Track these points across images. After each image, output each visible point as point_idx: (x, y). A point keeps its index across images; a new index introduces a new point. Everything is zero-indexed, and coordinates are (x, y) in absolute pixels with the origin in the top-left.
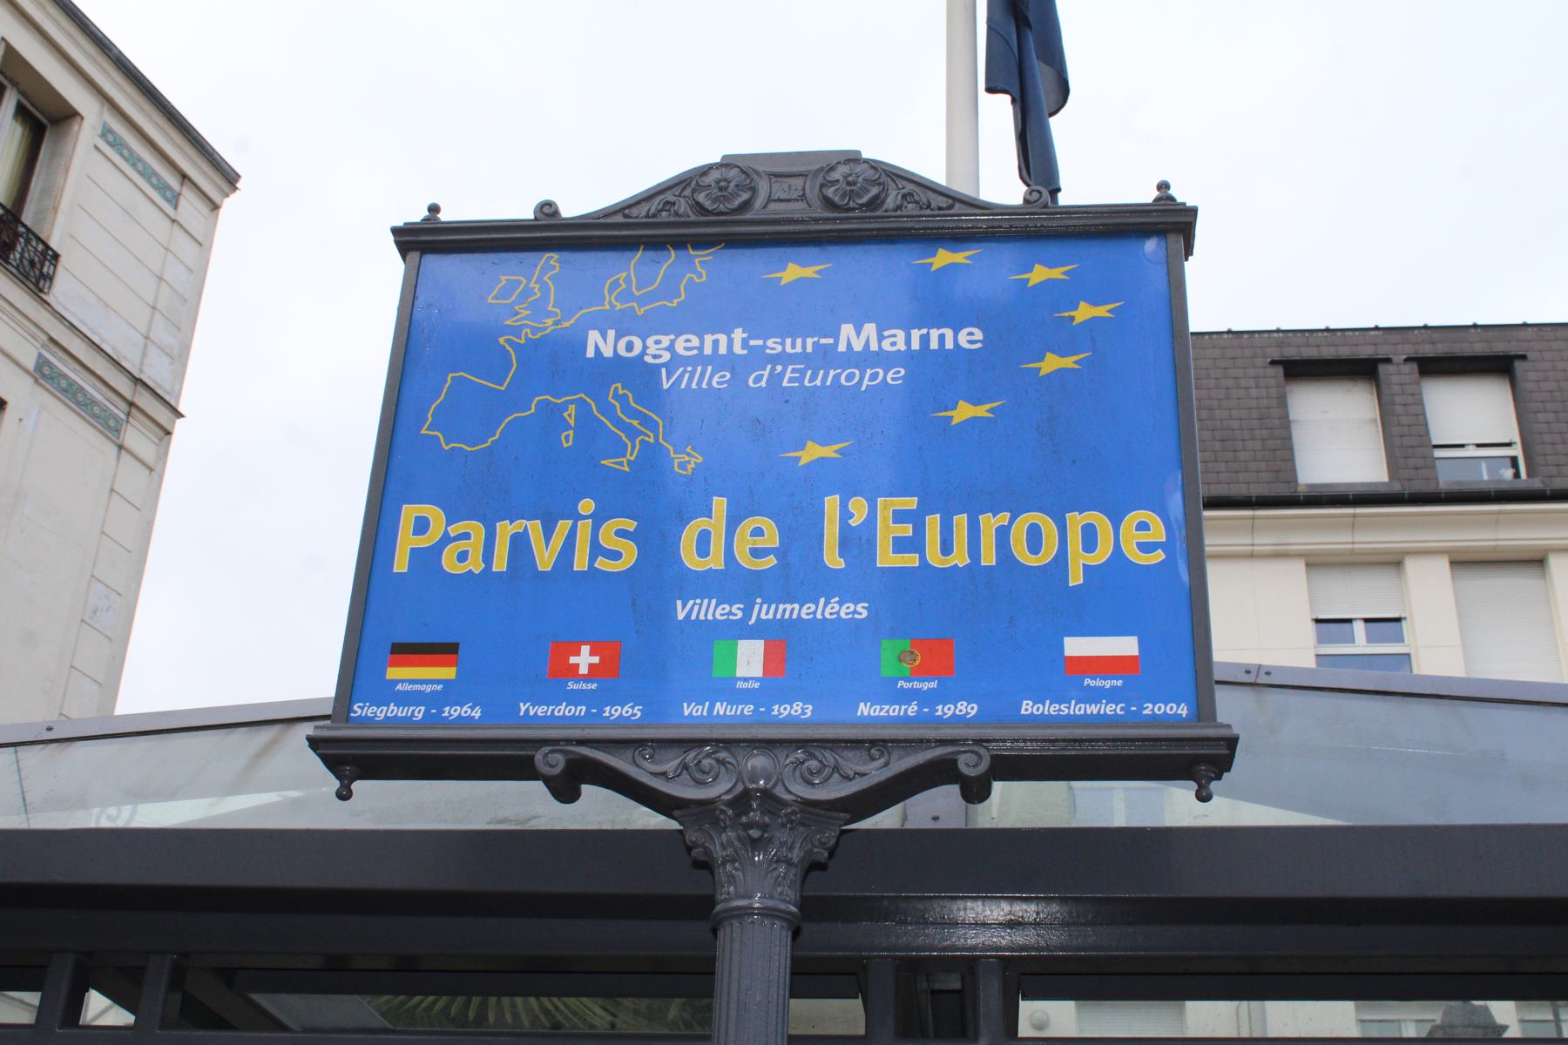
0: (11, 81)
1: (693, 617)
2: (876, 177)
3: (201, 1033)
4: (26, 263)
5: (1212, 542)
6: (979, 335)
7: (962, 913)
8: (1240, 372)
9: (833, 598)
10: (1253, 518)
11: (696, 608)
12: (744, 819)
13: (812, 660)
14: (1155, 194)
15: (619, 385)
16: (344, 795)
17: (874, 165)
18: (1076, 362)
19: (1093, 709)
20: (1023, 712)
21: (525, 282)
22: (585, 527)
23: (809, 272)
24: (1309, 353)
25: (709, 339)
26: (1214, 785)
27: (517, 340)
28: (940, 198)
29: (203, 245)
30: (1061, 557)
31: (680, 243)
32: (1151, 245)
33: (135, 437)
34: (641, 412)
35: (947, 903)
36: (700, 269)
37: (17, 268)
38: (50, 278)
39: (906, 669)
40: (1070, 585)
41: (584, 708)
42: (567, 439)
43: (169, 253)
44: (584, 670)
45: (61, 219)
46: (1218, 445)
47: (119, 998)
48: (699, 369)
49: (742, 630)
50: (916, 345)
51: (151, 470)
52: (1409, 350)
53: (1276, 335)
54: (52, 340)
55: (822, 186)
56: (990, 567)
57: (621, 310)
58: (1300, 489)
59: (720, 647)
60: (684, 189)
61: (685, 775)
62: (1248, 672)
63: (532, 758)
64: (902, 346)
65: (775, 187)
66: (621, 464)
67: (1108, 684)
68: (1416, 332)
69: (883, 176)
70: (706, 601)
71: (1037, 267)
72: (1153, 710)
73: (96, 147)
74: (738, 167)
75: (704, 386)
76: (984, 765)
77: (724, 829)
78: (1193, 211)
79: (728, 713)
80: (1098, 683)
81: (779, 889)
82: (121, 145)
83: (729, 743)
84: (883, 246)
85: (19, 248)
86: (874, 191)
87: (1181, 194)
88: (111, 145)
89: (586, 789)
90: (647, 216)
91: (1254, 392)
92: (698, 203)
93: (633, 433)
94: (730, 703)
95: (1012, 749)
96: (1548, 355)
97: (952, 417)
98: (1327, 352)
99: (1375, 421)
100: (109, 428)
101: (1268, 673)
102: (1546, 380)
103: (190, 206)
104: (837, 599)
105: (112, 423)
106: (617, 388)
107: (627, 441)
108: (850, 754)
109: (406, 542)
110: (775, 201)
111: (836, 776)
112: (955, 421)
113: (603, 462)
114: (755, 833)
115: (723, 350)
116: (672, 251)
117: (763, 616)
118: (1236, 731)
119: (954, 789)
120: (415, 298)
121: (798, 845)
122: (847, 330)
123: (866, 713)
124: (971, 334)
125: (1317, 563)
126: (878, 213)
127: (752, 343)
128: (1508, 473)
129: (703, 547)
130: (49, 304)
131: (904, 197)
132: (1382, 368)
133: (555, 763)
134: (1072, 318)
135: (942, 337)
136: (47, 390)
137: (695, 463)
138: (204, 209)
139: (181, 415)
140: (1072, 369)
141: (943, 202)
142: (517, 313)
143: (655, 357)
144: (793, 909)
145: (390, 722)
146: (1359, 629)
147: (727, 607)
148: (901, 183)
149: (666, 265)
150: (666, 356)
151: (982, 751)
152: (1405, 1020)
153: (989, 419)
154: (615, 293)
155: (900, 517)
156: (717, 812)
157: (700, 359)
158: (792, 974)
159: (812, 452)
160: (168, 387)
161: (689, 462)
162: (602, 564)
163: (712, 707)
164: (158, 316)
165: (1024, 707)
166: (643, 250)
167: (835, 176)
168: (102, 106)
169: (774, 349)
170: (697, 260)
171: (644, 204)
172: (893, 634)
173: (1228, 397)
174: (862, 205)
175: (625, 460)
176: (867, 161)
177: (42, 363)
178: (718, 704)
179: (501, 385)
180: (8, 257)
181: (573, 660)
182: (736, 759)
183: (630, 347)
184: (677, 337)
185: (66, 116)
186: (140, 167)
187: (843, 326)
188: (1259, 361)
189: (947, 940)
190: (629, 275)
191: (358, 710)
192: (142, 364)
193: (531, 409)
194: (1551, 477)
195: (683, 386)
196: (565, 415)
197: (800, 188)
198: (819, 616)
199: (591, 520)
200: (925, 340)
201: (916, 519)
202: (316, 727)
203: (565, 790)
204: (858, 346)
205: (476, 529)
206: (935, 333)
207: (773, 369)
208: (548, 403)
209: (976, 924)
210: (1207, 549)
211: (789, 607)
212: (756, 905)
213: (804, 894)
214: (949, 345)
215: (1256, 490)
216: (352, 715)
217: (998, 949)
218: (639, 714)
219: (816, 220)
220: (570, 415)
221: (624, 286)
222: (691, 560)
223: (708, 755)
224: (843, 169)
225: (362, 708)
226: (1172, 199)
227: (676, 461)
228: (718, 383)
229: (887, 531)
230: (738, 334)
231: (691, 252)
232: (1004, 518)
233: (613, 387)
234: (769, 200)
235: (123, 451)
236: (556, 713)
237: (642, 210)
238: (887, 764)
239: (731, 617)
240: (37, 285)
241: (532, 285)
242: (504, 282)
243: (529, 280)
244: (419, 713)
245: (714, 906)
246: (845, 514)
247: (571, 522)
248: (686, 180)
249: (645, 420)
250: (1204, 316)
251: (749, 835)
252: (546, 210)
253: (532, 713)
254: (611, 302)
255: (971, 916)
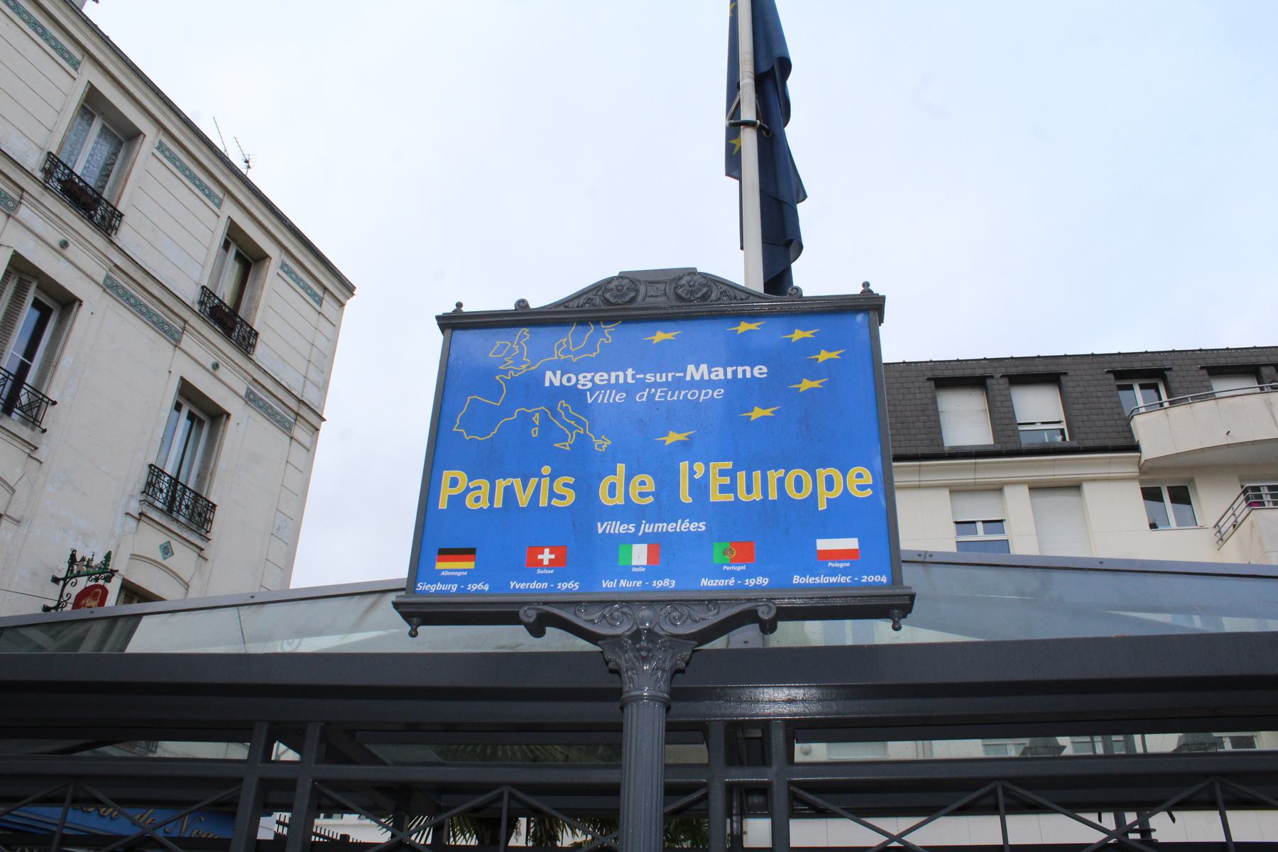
0: (233, 239)
1: (607, 532)
2: (706, 282)
3: (335, 766)
4: (241, 338)
5: (898, 480)
6: (765, 370)
7: (762, 695)
8: (910, 385)
9: (686, 519)
10: (920, 466)
11: (609, 526)
12: (638, 646)
13: (674, 554)
14: (862, 289)
15: (564, 401)
16: (413, 634)
17: (705, 276)
18: (820, 384)
19: (833, 580)
20: (794, 582)
21: (510, 345)
22: (545, 482)
23: (669, 336)
24: (948, 373)
25: (613, 374)
26: (902, 621)
27: (506, 377)
28: (742, 294)
29: (335, 326)
30: (814, 495)
31: (596, 322)
32: (860, 318)
33: (300, 432)
34: (575, 416)
35: (753, 690)
36: (607, 336)
37: (236, 341)
38: (253, 346)
39: (727, 559)
40: (820, 509)
41: (546, 584)
42: (535, 433)
43: (318, 332)
44: (546, 562)
45: (259, 314)
46: (899, 426)
47: (291, 746)
48: (608, 391)
49: (635, 539)
50: (729, 376)
51: (308, 450)
52: (1003, 371)
53: (929, 364)
54: (254, 379)
55: (675, 288)
56: (774, 501)
57: (565, 360)
58: (946, 449)
59: (622, 549)
60: (598, 291)
61: (604, 621)
62: (920, 555)
63: (517, 613)
64: (722, 377)
65: (649, 289)
66: (565, 446)
67: (841, 565)
68: (1007, 361)
69: (710, 282)
70: (614, 523)
71: (797, 331)
72: (867, 580)
73: (278, 274)
74: (628, 278)
75: (611, 401)
76: (773, 612)
77: (626, 652)
78: (883, 298)
79: (628, 586)
80: (837, 565)
81: (658, 685)
82: (291, 272)
83: (628, 603)
84: (710, 321)
85: (237, 330)
86: (705, 290)
87: (876, 289)
88: (286, 272)
89: (548, 629)
90: (578, 307)
91: (918, 396)
92: (606, 299)
93: (571, 429)
94: (629, 580)
95: (788, 603)
96: (1078, 372)
97: (750, 416)
98: (958, 373)
99: (986, 411)
100: (286, 428)
101: (931, 556)
102: (1079, 386)
103: (328, 306)
104: (688, 520)
105: (287, 425)
106: (562, 404)
107: (568, 433)
108: (697, 608)
109: (446, 492)
110: (649, 297)
111: (689, 620)
112: (752, 419)
113: (555, 445)
114: (644, 654)
115: (621, 381)
116: (592, 326)
117: (646, 531)
118: (914, 590)
119: (757, 626)
120: (449, 354)
121: (668, 660)
122: (691, 368)
123: (705, 585)
124: (761, 369)
125: (955, 490)
126: (706, 303)
127: (638, 376)
128: (1059, 438)
129: (612, 490)
130: (253, 360)
131: (721, 293)
132: (989, 381)
133: (530, 615)
134: (817, 359)
135: (744, 371)
136: (252, 407)
137: (607, 445)
138: (336, 306)
139: (324, 420)
140: (818, 388)
141: (743, 296)
142: (506, 362)
143: (583, 385)
144: (667, 696)
145: (438, 593)
146: (980, 526)
147: (626, 525)
148: (719, 285)
149: (589, 333)
150: (590, 385)
151: (772, 605)
152: (1009, 744)
153: (772, 417)
154: (561, 350)
155: (723, 473)
156: (623, 642)
157: (609, 386)
158: (667, 731)
159: (673, 437)
160: (316, 404)
161: (603, 444)
162: (555, 502)
163: (618, 582)
164: (311, 365)
165: (795, 579)
166: (576, 325)
167: (683, 282)
168: (282, 252)
169: (650, 380)
170: (606, 331)
171: (575, 300)
172: (720, 540)
173: (904, 399)
174: (698, 298)
175: (567, 443)
176: (700, 273)
177: (249, 392)
178: (622, 581)
179: (498, 403)
180: (231, 335)
181: (540, 557)
182: (632, 611)
183: (569, 380)
184: (596, 374)
185: (262, 257)
186: (301, 284)
187: (689, 366)
188: (921, 379)
189: (753, 710)
190: (568, 339)
191: (421, 587)
192: (303, 392)
193: (461, 432)
194: (1082, 440)
195: (599, 401)
196: (534, 418)
197: (663, 289)
198: (678, 530)
199: (548, 478)
200: (735, 373)
201: (732, 474)
202: (397, 597)
203: (537, 630)
204: (697, 377)
205: (485, 484)
206: (740, 369)
207: (650, 391)
208: (524, 412)
209: (770, 701)
210: (895, 484)
211: (661, 525)
212: (646, 694)
213: (672, 686)
214: (748, 376)
215: (921, 451)
216: (417, 589)
217: (782, 715)
218: (578, 587)
219: (672, 307)
220: (536, 419)
221: (565, 346)
222: (605, 500)
223: (617, 610)
224: (687, 278)
225: (422, 585)
226: (871, 291)
227: (596, 444)
228: (619, 399)
229: (716, 481)
230: (630, 372)
231: (603, 326)
232: (781, 472)
233: (560, 403)
234: (646, 296)
235: (293, 441)
236: (531, 587)
237: (576, 303)
238: (718, 613)
239: (628, 531)
240: (246, 350)
241: (514, 346)
242: (498, 345)
243: (513, 344)
244: (454, 588)
245: (622, 695)
246: (692, 472)
247: (537, 479)
248: (598, 287)
249: (578, 421)
250: (890, 354)
251: (641, 655)
252: (521, 304)
253: (517, 587)
254: (558, 355)
255: (767, 697)
